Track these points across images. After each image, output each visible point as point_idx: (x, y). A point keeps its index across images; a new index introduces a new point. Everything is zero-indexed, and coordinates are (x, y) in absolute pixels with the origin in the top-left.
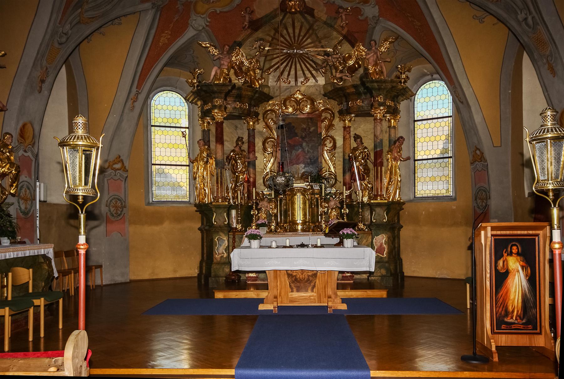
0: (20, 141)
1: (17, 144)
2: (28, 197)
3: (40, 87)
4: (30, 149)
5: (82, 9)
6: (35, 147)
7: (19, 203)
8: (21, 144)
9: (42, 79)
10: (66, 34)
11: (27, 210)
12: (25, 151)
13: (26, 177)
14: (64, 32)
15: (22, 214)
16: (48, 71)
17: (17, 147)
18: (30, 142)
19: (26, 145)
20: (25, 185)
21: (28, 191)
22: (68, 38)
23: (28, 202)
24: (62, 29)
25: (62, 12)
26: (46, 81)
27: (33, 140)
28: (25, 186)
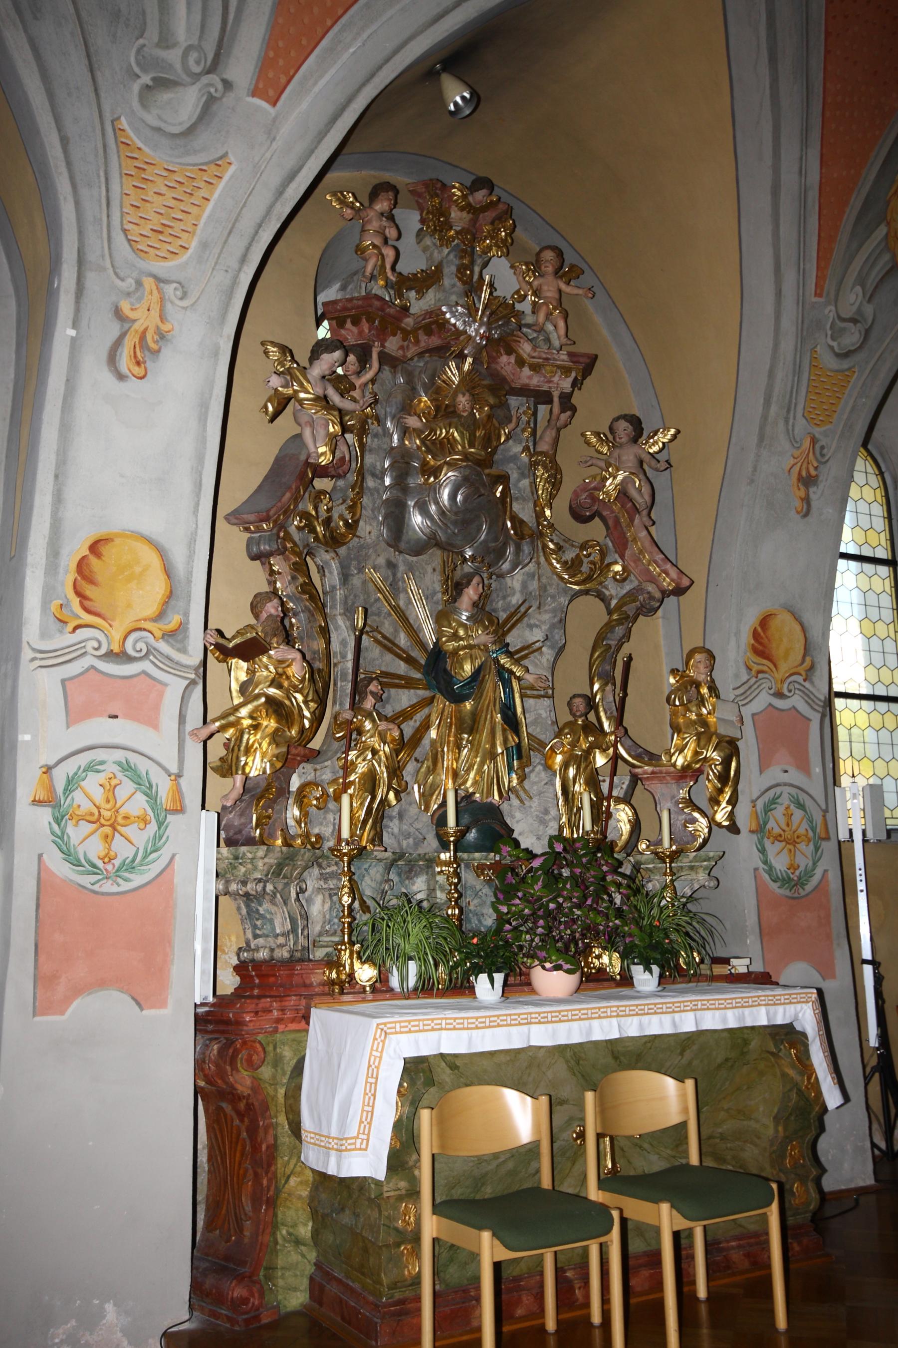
0: (756, 668)
1: (745, 677)
2: (801, 831)
3: (802, 500)
4: (797, 686)
5: (888, 224)
6: (816, 680)
7: (763, 851)
8: (760, 676)
9: (804, 474)
10: (854, 321)
11: (797, 873)
12: (779, 695)
13: (786, 771)
14: (844, 316)
15: (778, 884)
16: (822, 448)
17: (746, 687)
18: (797, 667)
19: (778, 676)
20: (785, 796)
21: (798, 814)
22: (867, 332)
23: (802, 846)
24: (833, 308)
25: (815, 255)
26: (820, 479)
27: (808, 659)
28: (785, 800)
